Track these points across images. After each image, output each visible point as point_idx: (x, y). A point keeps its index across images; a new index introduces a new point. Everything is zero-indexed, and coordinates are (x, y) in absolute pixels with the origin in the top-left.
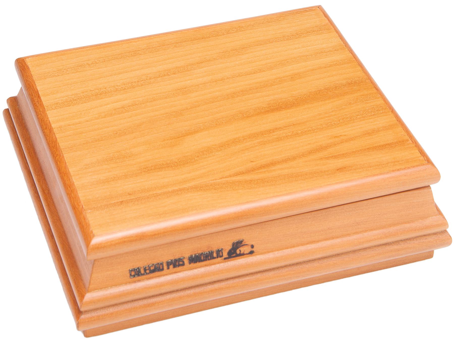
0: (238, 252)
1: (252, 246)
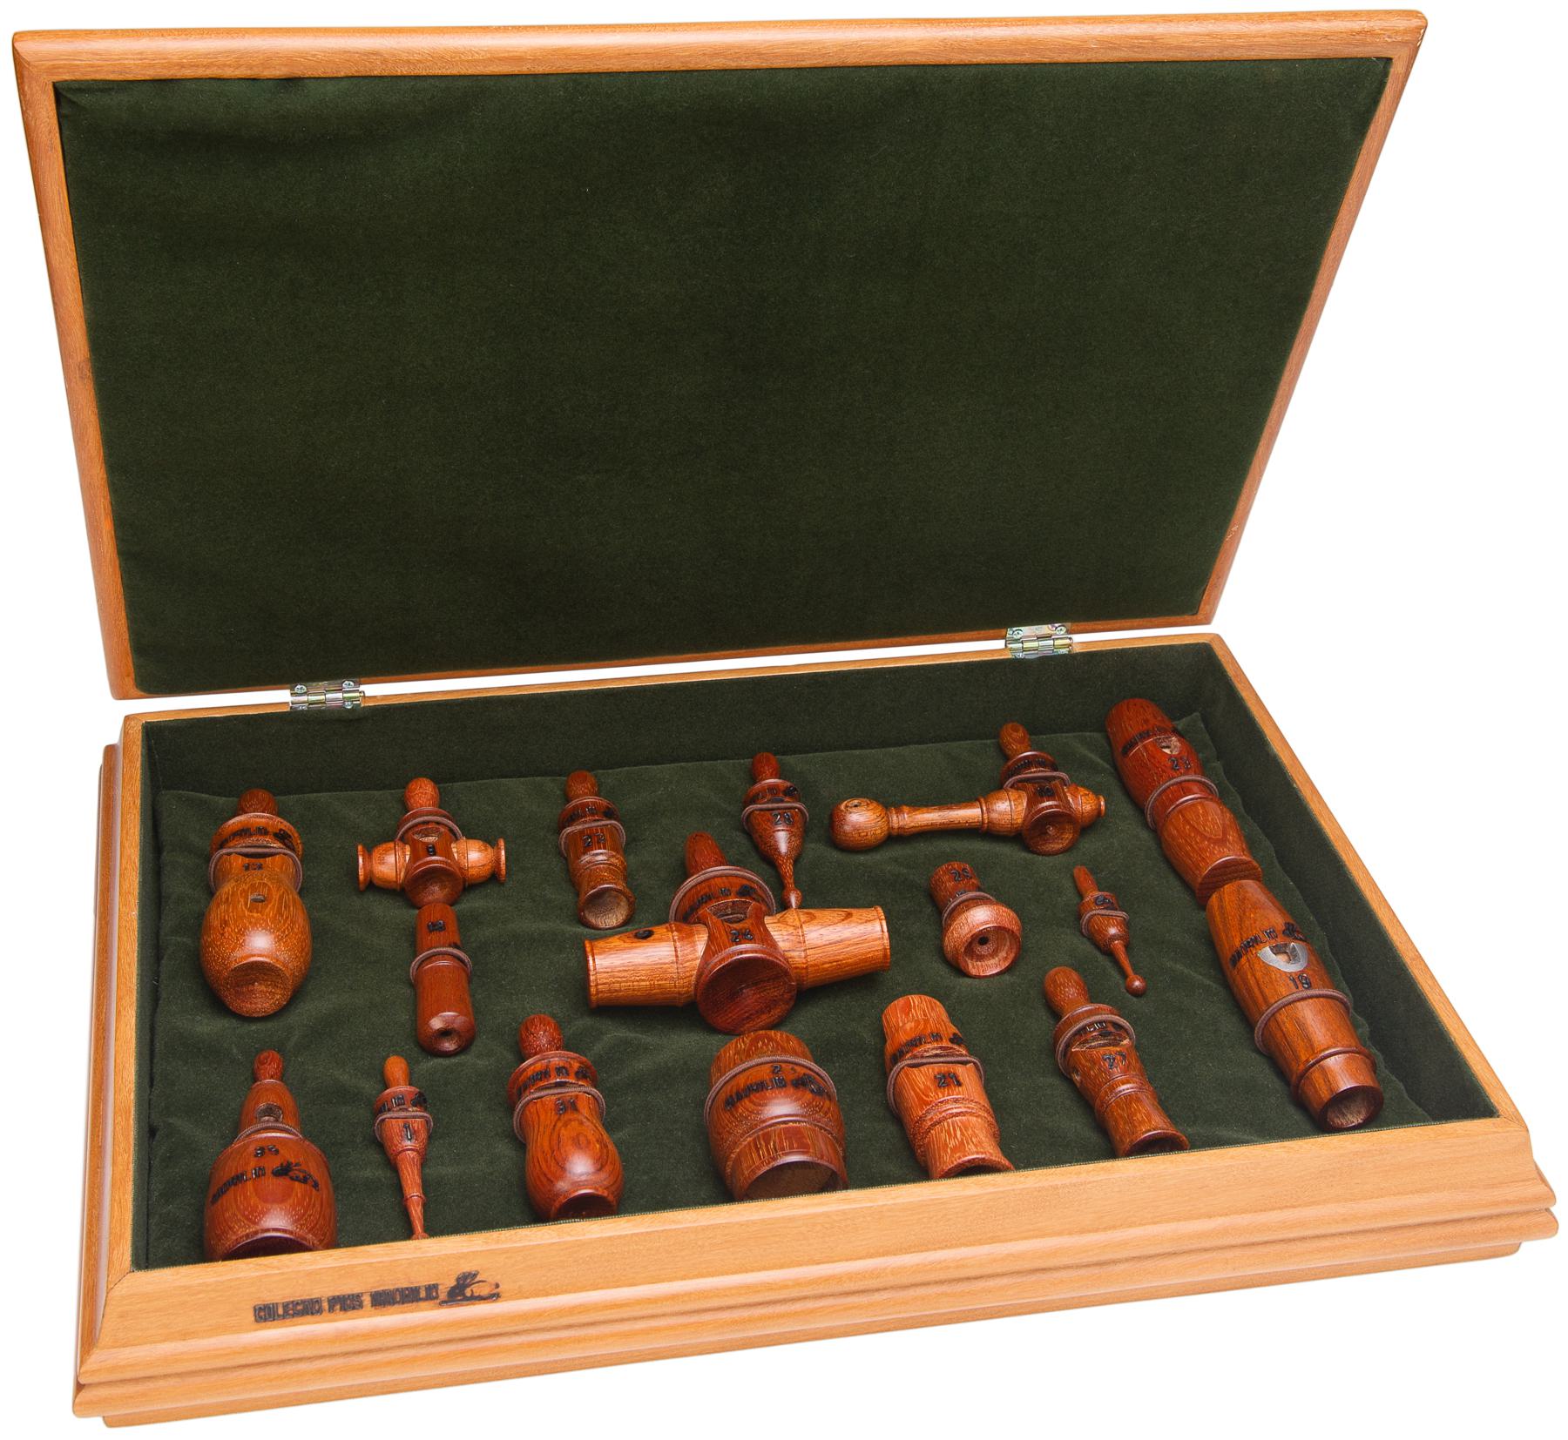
0: (468, 1293)
1: (497, 1286)
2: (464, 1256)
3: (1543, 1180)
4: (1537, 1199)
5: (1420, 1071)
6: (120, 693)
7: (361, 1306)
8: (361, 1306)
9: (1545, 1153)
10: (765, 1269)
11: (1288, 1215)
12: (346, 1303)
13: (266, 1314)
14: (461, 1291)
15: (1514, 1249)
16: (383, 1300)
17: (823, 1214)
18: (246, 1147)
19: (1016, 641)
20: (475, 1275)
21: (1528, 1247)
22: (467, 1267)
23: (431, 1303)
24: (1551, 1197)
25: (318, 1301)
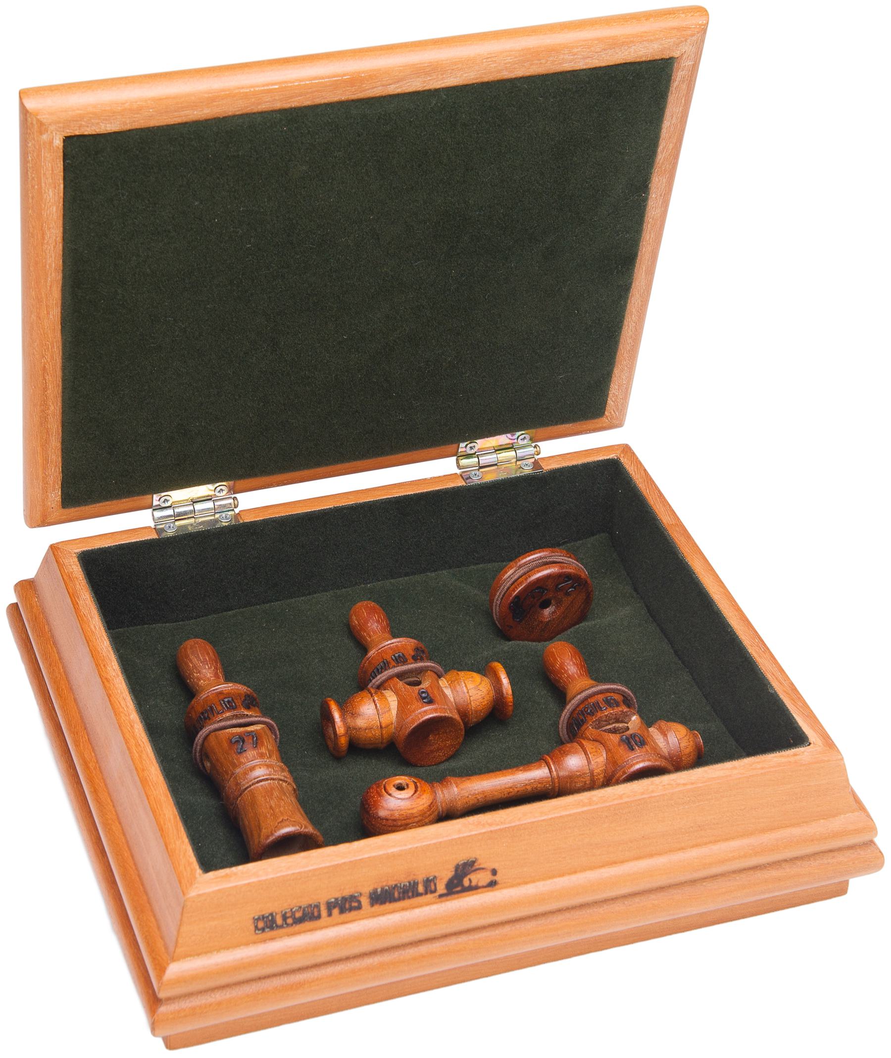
0: (466, 882)
1: (494, 872)
2: (461, 841)
3: (861, 807)
4: (858, 831)
5: (741, 709)
6: (38, 518)
7: (359, 907)
8: (359, 907)
9: (860, 780)
10: (651, 855)
11: (796, 831)
12: (346, 905)
13: (268, 924)
14: (459, 882)
15: (841, 890)
16: (383, 897)
17: (245, 885)
18: (435, 710)
19: (468, 456)
20: (474, 862)
21: (856, 884)
22: (462, 857)
23: (430, 897)
24: (871, 828)
25: (414, 885)
